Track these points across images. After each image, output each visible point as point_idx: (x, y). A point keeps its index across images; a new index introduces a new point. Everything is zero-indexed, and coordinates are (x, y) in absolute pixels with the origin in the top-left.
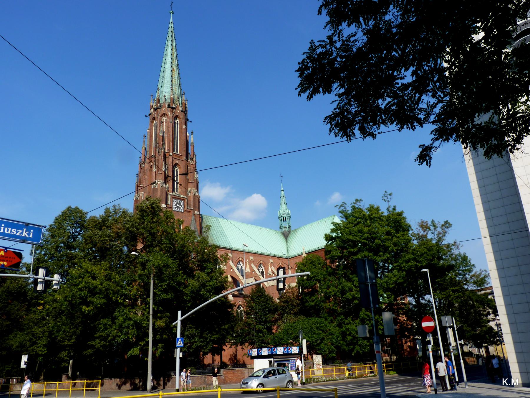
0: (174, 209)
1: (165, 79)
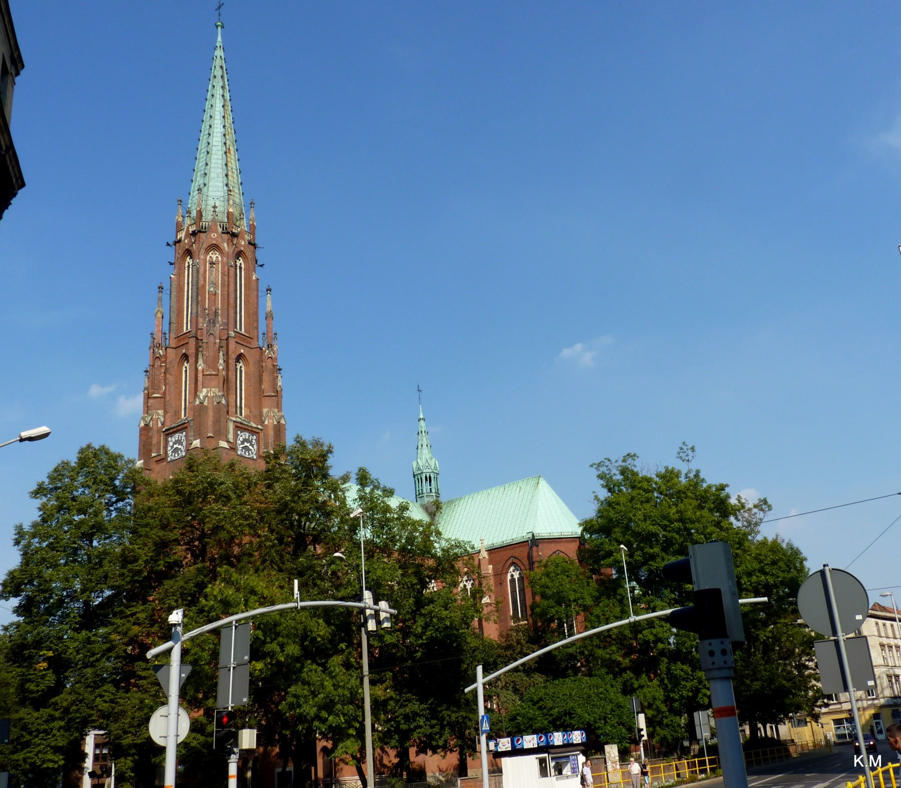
0: (239, 453)
1: (212, 170)
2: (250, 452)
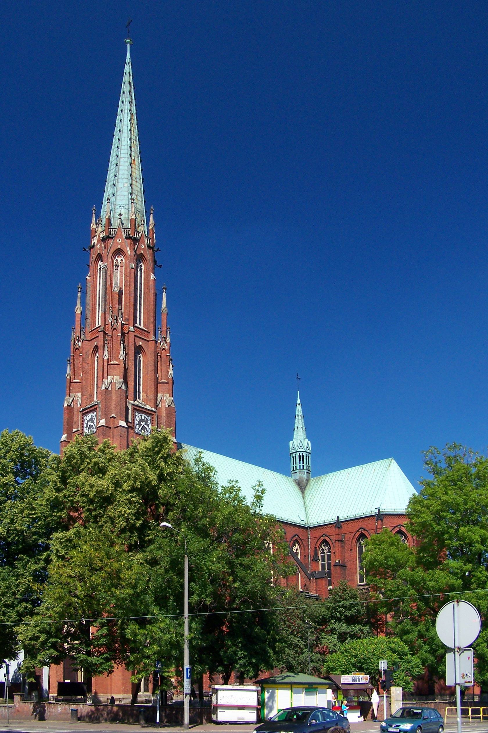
0: (136, 431)
1: (120, 180)
2: (146, 430)
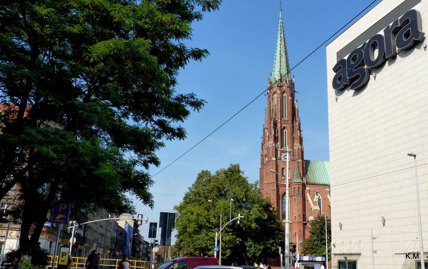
0: (282, 160)
